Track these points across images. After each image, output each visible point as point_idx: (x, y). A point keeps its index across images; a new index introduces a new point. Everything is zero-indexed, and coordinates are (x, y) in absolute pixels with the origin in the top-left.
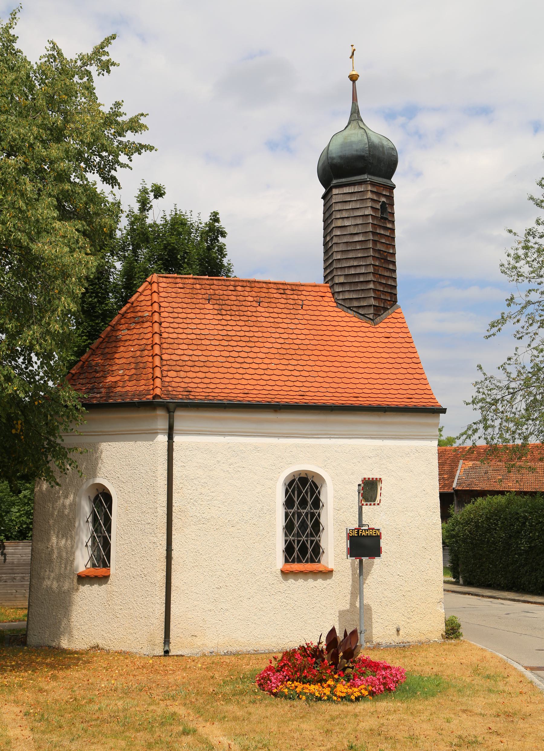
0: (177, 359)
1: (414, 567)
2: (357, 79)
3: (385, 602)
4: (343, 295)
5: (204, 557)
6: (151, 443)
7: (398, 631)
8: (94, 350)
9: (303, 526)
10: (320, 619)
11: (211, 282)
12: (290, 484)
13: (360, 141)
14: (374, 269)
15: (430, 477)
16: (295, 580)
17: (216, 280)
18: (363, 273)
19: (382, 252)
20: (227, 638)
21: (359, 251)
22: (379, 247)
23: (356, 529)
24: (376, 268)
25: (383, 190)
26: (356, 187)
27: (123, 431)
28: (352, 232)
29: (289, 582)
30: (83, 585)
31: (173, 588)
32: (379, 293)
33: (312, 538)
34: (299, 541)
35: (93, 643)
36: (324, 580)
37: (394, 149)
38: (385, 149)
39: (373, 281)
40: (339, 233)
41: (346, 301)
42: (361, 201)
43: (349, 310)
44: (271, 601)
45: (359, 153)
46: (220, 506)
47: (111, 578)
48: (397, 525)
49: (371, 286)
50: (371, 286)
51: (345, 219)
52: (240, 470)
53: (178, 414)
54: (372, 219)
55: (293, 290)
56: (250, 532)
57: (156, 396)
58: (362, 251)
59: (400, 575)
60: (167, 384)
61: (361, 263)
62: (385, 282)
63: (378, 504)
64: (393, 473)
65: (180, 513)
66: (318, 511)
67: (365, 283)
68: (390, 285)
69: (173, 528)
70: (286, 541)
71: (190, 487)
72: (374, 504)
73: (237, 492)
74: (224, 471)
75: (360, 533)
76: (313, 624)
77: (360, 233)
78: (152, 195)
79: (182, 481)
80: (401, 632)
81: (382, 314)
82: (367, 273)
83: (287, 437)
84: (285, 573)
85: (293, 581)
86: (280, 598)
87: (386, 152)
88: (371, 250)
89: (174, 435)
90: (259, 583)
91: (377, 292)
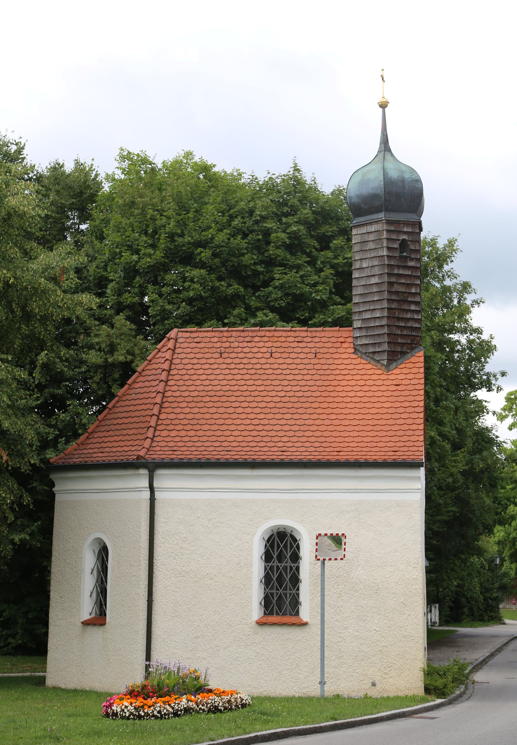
1: (392, 623)
2: (386, 106)
3: (361, 656)
5: (184, 608)
9: (280, 580)
12: (295, 540)
15: (411, 531)
18: (379, 317)
19: (400, 294)
21: (376, 294)
25: (404, 227)
26: (373, 226)
33: (291, 592)
37: (418, 181)
40: (357, 276)
44: (247, 652)
45: (374, 192)
46: (199, 559)
48: (376, 580)
54: (388, 260)
56: (227, 585)
57: (139, 457)
58: (378, 293)
59: (377, 629)
62: (403, 325)
63: (342, 559)
66: (296, 565)
70: (265, 593)
72: (336, 559)
74: (204, 527)
84: (260, 623)
86: (256, 648)
87: (407, 186)
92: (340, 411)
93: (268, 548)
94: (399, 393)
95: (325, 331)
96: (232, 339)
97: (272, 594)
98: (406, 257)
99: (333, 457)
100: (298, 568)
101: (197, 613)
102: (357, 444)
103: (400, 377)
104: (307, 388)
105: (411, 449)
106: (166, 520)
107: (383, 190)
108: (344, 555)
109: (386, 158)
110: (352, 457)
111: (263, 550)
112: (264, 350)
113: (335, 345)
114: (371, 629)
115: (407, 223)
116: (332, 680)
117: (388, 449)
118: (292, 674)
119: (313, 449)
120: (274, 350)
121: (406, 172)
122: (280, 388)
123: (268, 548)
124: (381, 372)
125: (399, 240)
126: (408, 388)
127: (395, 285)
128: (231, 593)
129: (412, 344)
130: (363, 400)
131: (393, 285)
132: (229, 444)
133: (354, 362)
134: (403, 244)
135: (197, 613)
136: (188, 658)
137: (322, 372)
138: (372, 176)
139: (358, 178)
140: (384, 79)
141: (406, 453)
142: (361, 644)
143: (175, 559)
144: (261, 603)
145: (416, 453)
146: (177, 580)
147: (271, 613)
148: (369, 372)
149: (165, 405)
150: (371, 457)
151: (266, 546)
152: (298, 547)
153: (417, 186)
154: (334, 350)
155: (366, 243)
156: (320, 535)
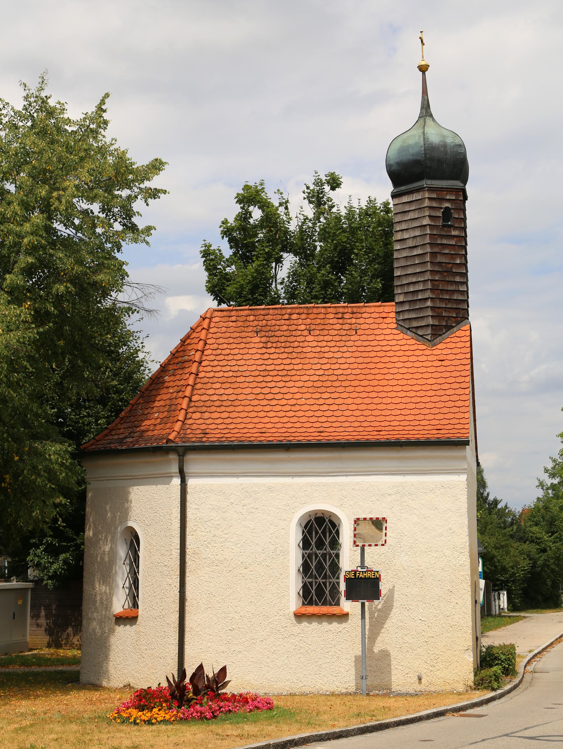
0: (206, 399)
1: (438, 612)
2: (427, 70)
3: (406, 648)
4: (403, 316)
5: (218, 599)
6: (168, 486)
7: (420, 679)
8: (143, 393)
9: (320, 567)
10: (335, 664)
11: (267, 312)
12: (334, 525)
13: (416, 144)
14: (433, 285)
15: (457, 514)
16: (308, 623)
17: (273, 309)
18: (422, 290)
19: (444, 264)
20: (240, 681)
21: (418, 265)
22: (439, 259)
23: (352, 571)
24: (436, 283)
25: (447, 194)
27: (113, 477)
28: (411, 246)
29: (302, 624)
30: (119, 626)
31: (187, 629)
32: (440, 310)
34: (316, 583)
35: (126, 682)
36: (339, 624)
37: (462, 146)
38: (448, 147)
39: (431, 298)
40: (398, 248)
41: (406, 321)
42: (419, 210)
43: (408, 332)
44: (285, 644)
45: (415, 158)
46: (233, 547)
47: (139, 619)
49: (429, 303)
50: (429, 303)
51: (404, 231)
52: (253, 511)
53: (190, 457)
54: (430, 229)
55: (353, 313)
56: (263, 574)
58: (421, 265)
59: (422, 619)
60: (187, 426)
61: (420, 279)
62: (448, 297)
63: (383, 545)
64: (415, 511)
65: (194, 555)
66: (335, 552)
67: (423, 301)
68: (456, 300)
69: (187, 570)
70: (303, 582)
71: (204, 529)
72: (376, 545)
73: (250, 533)
75: (357, 575)
76: (327, 669)
77: (418, 246)
78: (327, 188)
79: (196, 523)
80: (423, 681)
81: (444, 333)
82: (425, 290)
83: (301, 476)
84: (299, 616)
85: (307, 624)
86: (294, 641)
87: (449, 151)
88: (429, 263)
89: (186, 478)
90: (272, 626)
91: (437, 310)
92: (381, 389)
93: (306, 534)
94: (444, 369)
95: (366, 307)
96: (270, 317)
97: (311, 583)
98: (450, 226)
99: (373, 437)
100: (338, 556)
101: (231, 604)
102: (398, 423)
103: (444, 352)
104: (346, 366)
105: (456, 427)
106: (197, 507)
107: (423, 156)
108: (386, 540)
109: (427, 123)
110: (393, 437)
111: (300, 537)
112: (303, 327)
113: (377, 321)
114: (416, 618)
115: (450, 190)
116: (376, 674)
117: (432, 427)
118: (332, 667)
119: (352, 429)
120: (313, 327)
121: (448, 137)
122: (318, 366)
123: (306, 534)
124: (425, 347)
125: (442, 208)
126: (453, 363)
127: (439, 256)
128: (267, 583)
129: (458, 317)
130: (405, 376)
131: (437, 257)
132: (263, 425)
133: (396, 337)
134: (447, 214)
135: (231, 604)
136: (223, 652)
137: (362, 349)
138: (411, 142)
139: (397, 145)
140: (424, 42)
141: (451, 431)
142: (406, 635)
143: (208, 547)
144: (299, 593)
145: (461, 431)
146: (211, 570)
147: (310, 603)
148: (412, 348)
149: (198, 386)
150: (413, 436)
151: (303, 532)
152: (338, 533)
153: (460, 151)
154: (376, 326)
155: (423, 209)
156: (358, 519)
